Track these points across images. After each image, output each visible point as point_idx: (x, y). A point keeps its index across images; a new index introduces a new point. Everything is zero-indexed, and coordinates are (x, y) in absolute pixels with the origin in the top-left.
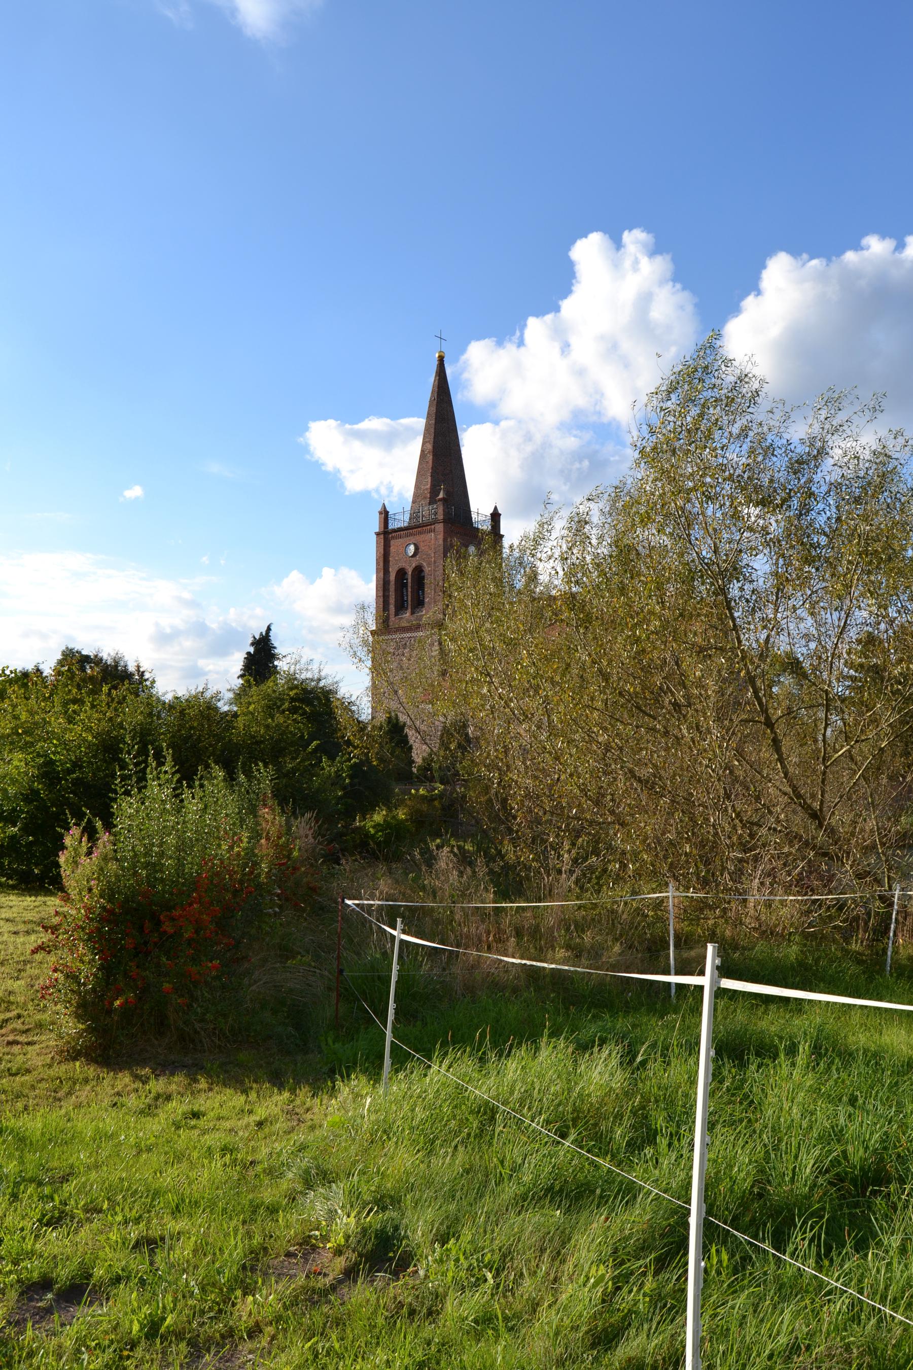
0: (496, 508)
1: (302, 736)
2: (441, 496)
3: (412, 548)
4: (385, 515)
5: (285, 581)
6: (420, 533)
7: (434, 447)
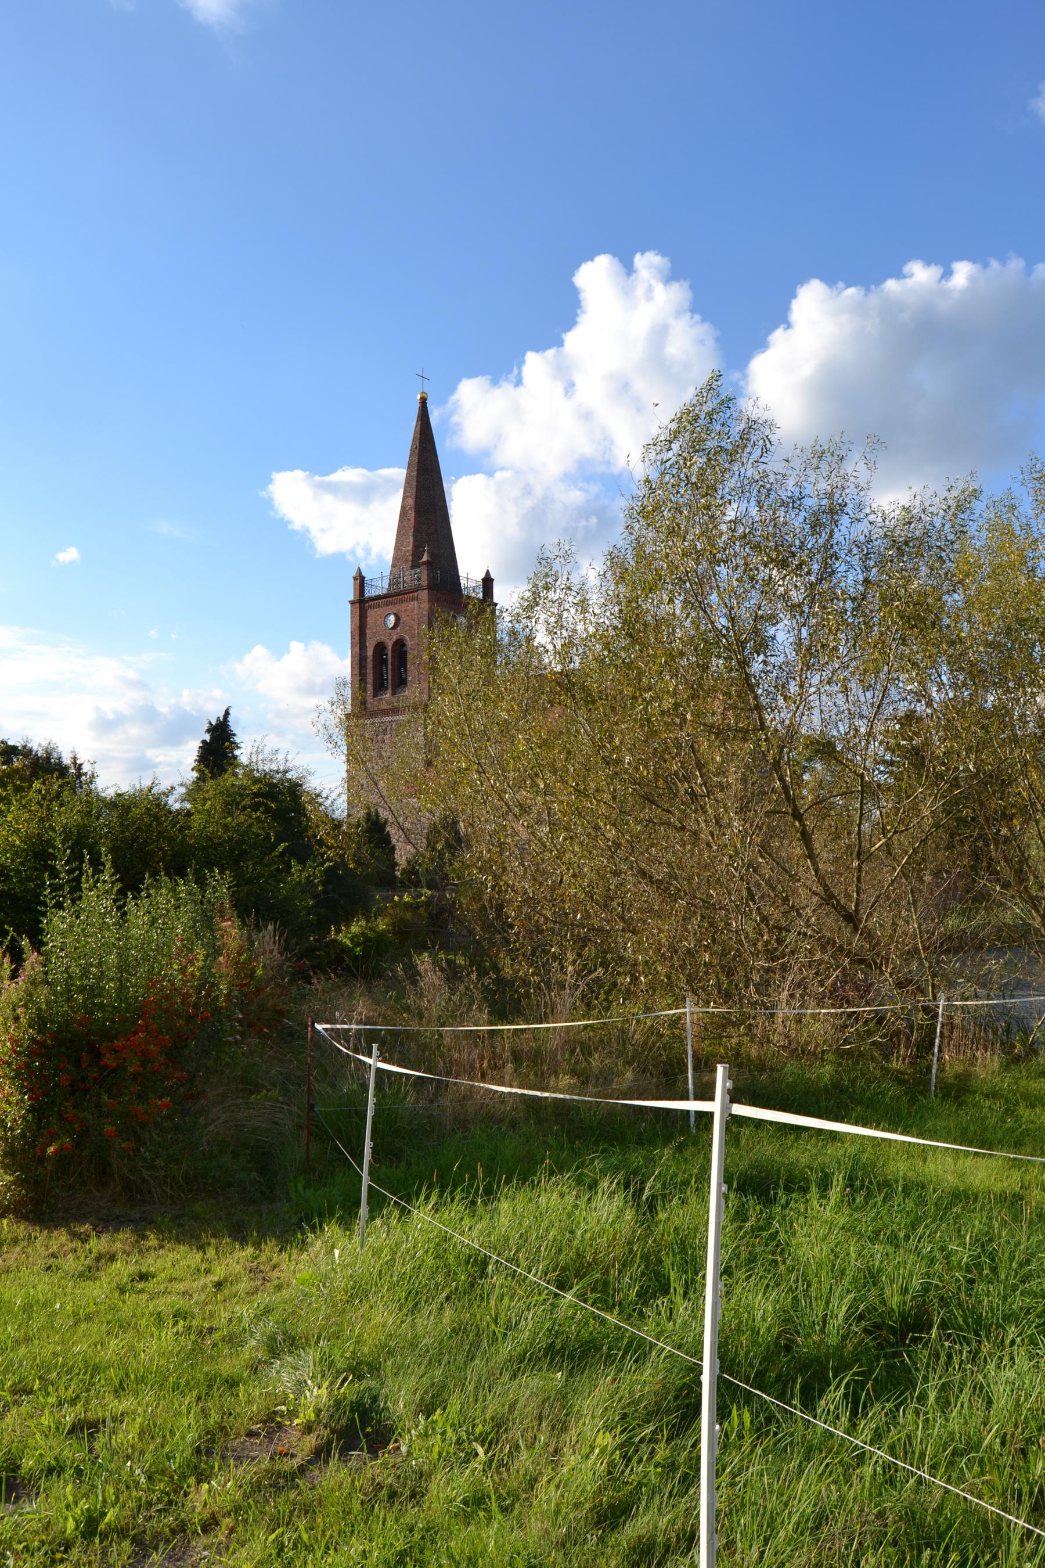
0: (488, 572)
1: (267, 837)
2: (425, 558)
4: (360, 581)
6: (402, 601)
7: (416, 502)
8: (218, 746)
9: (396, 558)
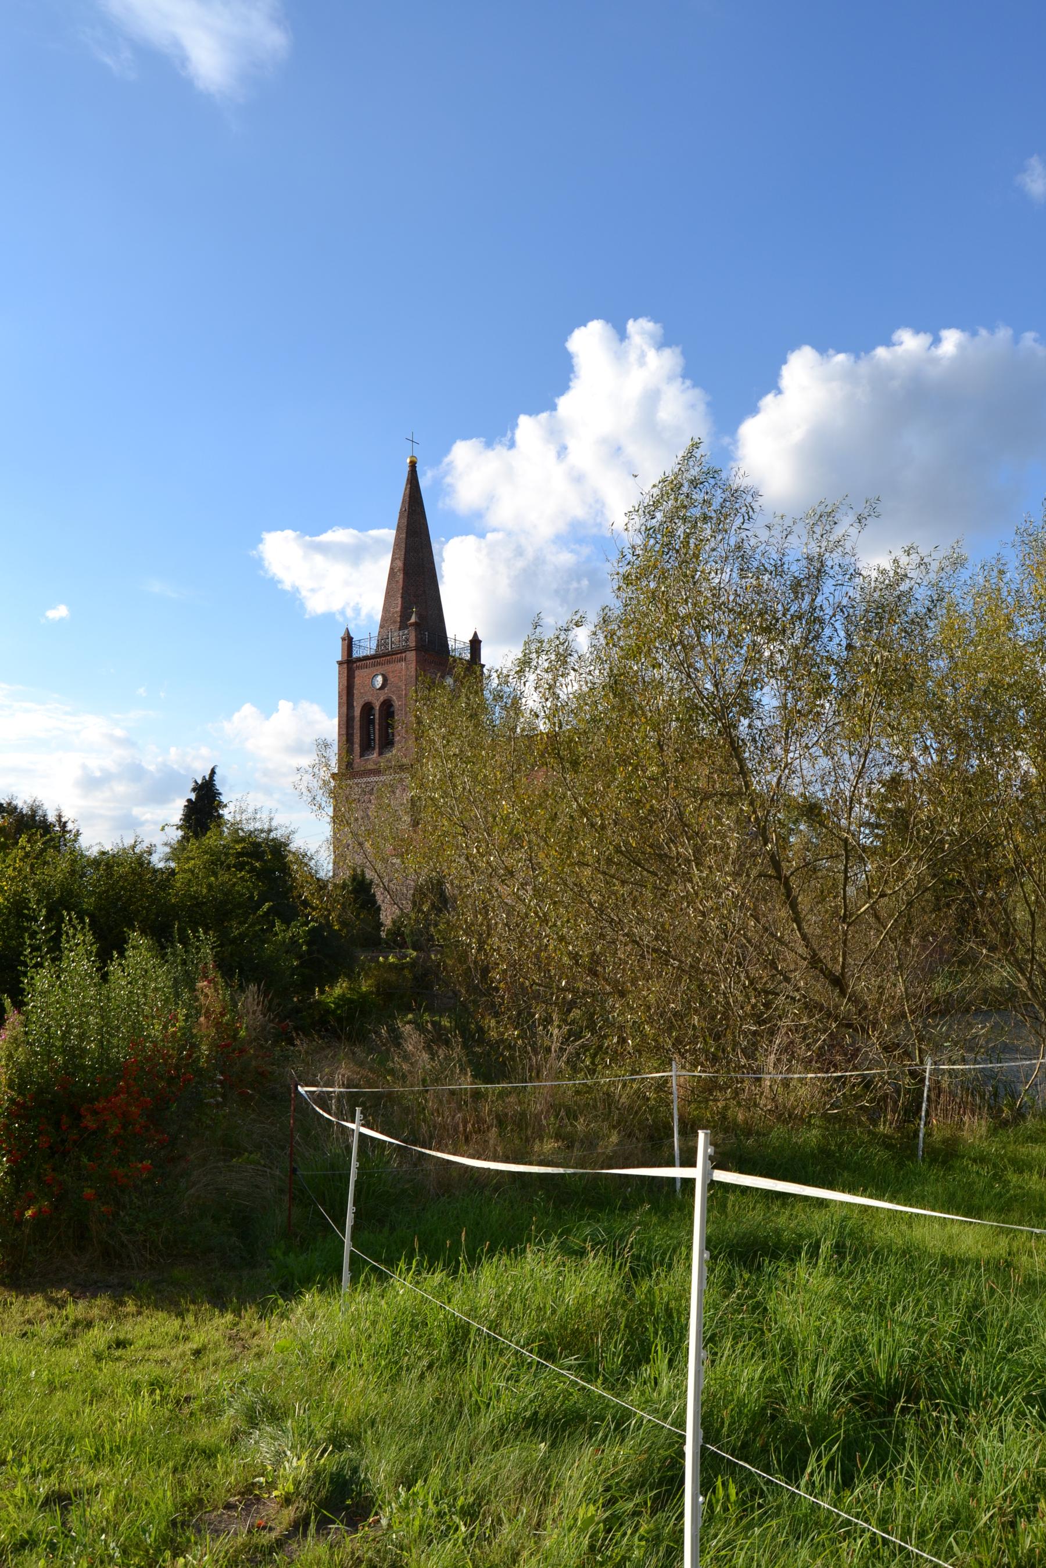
0: (475, 634)
1: (252, 897)
2: (413, 620)
3: (380, 679)
4: (349, 641)
5: (236, 717)
6: (389, 662)
7: (405, 564)
8: (204, 805)
9: (384, 619)
